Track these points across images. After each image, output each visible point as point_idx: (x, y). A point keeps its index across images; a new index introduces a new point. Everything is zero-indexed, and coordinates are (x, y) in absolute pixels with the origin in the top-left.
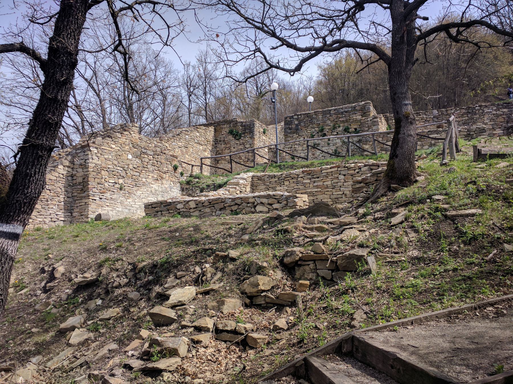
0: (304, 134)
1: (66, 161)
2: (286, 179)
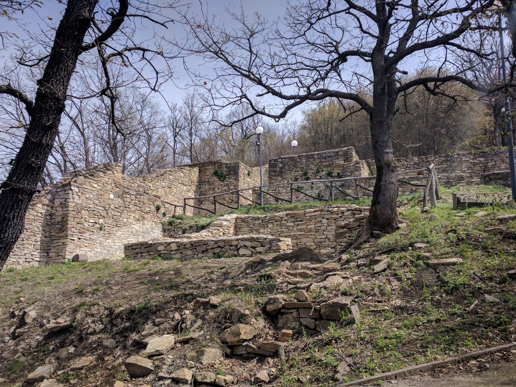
0: (288, 177)
1: (45, 199)
2: (270, 222)
